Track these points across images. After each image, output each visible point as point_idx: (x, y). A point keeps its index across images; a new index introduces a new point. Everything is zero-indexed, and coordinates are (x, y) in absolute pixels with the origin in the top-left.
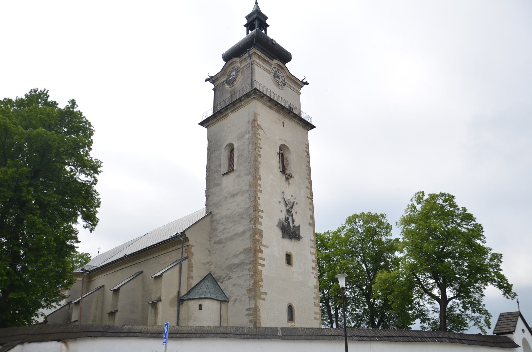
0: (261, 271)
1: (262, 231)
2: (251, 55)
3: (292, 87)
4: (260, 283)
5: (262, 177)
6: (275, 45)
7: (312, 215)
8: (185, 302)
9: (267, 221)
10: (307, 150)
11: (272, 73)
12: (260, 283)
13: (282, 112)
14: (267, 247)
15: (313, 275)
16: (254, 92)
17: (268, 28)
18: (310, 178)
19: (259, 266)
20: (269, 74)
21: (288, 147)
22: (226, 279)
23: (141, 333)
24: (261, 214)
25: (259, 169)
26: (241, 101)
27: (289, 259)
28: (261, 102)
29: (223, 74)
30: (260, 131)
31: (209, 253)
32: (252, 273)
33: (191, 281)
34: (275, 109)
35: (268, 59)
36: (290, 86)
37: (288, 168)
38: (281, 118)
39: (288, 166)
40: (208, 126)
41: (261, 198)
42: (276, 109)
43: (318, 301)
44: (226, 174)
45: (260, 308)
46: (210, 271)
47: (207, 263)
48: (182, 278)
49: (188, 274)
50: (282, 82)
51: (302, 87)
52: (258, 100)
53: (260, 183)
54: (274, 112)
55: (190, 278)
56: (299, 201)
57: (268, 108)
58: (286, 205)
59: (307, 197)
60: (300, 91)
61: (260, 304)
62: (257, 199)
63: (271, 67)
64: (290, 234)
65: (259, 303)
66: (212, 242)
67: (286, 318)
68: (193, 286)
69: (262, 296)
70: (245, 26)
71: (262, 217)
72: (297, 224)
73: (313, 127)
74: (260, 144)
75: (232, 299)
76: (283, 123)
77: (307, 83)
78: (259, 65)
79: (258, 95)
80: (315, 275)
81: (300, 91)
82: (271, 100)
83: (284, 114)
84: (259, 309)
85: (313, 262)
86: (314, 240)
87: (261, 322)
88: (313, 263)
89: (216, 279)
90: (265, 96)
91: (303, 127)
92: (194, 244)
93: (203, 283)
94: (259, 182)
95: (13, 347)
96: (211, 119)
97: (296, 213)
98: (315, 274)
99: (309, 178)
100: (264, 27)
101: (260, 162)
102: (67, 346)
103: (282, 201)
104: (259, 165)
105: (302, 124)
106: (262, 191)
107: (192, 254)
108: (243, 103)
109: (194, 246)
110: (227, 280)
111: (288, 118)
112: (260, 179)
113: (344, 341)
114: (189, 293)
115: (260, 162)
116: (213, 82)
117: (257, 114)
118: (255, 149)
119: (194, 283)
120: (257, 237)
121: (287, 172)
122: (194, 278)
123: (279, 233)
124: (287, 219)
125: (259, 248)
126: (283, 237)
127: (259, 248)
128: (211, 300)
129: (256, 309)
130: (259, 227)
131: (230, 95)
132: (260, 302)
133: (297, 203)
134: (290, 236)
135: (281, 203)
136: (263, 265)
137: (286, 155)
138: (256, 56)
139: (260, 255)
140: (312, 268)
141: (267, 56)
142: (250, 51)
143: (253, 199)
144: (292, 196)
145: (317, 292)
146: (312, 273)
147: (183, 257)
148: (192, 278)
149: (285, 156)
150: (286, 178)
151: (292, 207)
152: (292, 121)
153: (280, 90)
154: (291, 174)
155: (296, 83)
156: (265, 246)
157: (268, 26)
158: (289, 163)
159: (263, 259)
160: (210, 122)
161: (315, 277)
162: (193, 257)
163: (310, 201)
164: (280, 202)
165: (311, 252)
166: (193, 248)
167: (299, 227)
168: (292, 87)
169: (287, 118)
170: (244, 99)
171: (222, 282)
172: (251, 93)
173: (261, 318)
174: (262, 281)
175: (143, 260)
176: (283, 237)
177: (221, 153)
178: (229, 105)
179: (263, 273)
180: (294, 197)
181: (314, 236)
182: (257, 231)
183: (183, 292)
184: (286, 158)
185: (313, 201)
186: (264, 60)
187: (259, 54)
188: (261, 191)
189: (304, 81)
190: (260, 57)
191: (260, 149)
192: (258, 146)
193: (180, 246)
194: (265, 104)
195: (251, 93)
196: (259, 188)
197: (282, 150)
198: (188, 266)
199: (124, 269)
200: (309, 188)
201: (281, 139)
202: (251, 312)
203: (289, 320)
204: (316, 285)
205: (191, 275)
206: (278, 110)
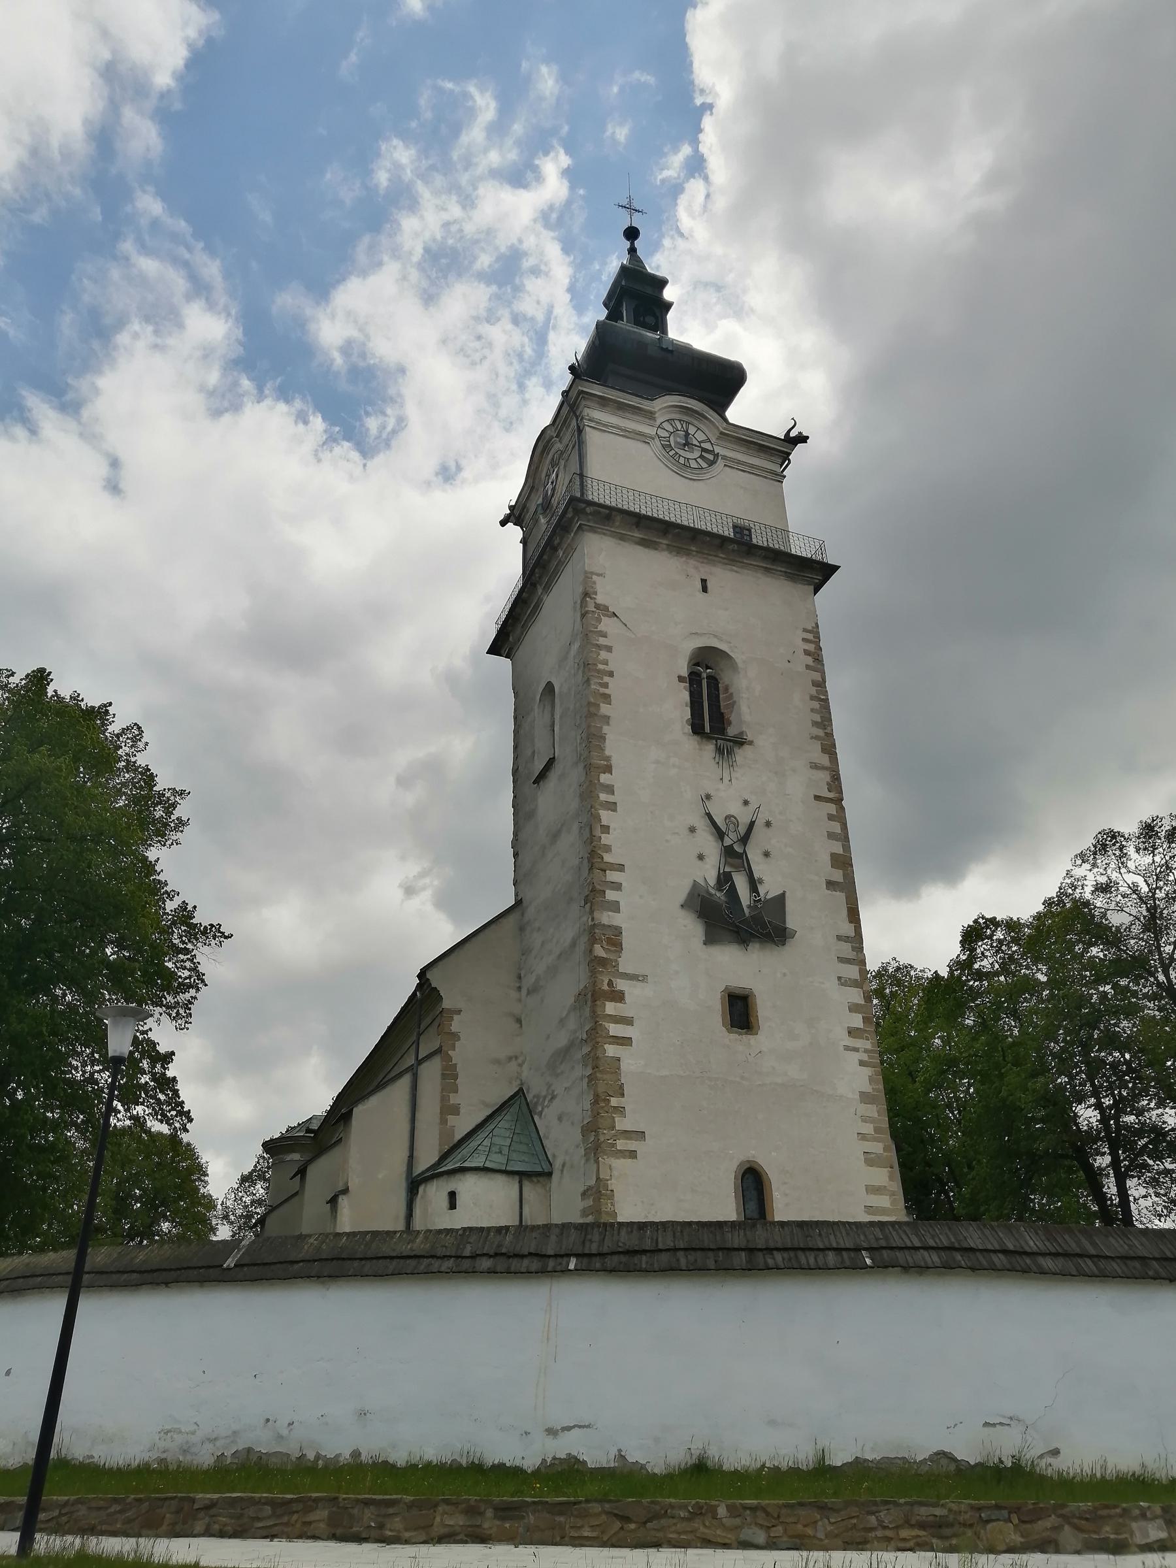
0: (619, 1060)
1: (618, 931)
3: (744, 463)
4: (614, 1102)
5: (613, 762)
6: (672, 351)
7: (841, 851)
9: (641, 897)
11: (657, 440)
12: (614, 1102)
13: (694, 549)
14: (642, 981)
15: (855, 1057)
16: (574, 509)
18: (830, 735)
19: (606, 1046)
20: (646, 445)
24: (612, 876)
25: (603, 738)
28: (611, 536)
29: (533, 487)
30: (606, 624)
31: (519, 1025)
32: (589, 1071)
34: (665, 546)
35: (633, 401)
36: (732, 464)
38: (696, 568)
39: (732, 712)
40: (511, 649)
41: (612, 826)
42: (667, 545)
45: (613, 1184)
46: (522, 1084)
47: (510, 1059)
49: (444, 1099)
50: (701, 457)
52: (595, 532)
53: (608, 783)
54: (666, 553)
55: (449, 1110)
58: (720, 834)
59: (817, 798)
61: (615, 1173)
62: (597, 832)
63: (654, 419)
64: (737, 927)
65: (611, 1169)
66: (524, 991)
68: (458, 1137)
69: (621, 1144)
71: (617, 887)
72: (769, 889)
77: (802, 439)
78: (604, 425)
79: (590, 517)
82: (639, 521)
83: (704, 554)
84: (610, 1188)
85: (850, 1010)
90: (614, 513)
94: (604, 778)
96: (510, 628)
98: (866, 1051)
101: (606, 719)
103: (702, 824)
105: (783, 569)
106: (616, 803)
107: (455, 1036)
108: (561, 553)
109: (459, 1012)
111: (725, 561)
112: (608, 769)
113: (68, 1290)
114: (444, 1157)
115: (609, 717)
117: (592, 573)
118: (588, 681)
119: (462, 1125)
120: (599, 951)
121: (731, 731)
122: (462, 1111)
123: (692, 928)
124: (724, 879)
125: (606, 987)
126: (711, 939)
127: (606, 987)
128: (482, 1173)
129: (600, 1191)
130: (606, 918)
132: (613, 1165)
134: (737, 933)
136: (626, 1041)
137: (725, 678)
138: (588, 403)
140: (849, 1032)
141: (617, 389)
143: (587, 834)
144: (746, 803)
145: (876, 1115)
146: (847, 1048)
148: (455, 1110)
149: (723, 683)
150: (719, 751)
151: (745, 839)
152: (742, 567)
153: (695, 483)
154: (742, 733)
156: (633, 977)
158: (735, 702)
159: (628, 1021)
161: (862, 1063)
163: (832, 808)
164: (692, 830)
165: (839, 978)
166: (456, 1017)
167: (781, 899)
169: (720, 562)
170: (561, 539)
174: (623, 1095)
176: (711, 939)
177: (534, 720)
179: (624, 1066)
182: (597, 931)
184: (727, 689)
185: (843, 809)
186: (621, 407)
187: (601, 394)
188: (612, 807)
189: (793, 434)
190: (603, 402)
191: (606, 679)
192: (599, 671)
194: (622, 538)
195: (569, 515)
196: (603, 797)
197: (708, 667)
200: (823, 768)
204: (868, 1088)
206: (674, 544)
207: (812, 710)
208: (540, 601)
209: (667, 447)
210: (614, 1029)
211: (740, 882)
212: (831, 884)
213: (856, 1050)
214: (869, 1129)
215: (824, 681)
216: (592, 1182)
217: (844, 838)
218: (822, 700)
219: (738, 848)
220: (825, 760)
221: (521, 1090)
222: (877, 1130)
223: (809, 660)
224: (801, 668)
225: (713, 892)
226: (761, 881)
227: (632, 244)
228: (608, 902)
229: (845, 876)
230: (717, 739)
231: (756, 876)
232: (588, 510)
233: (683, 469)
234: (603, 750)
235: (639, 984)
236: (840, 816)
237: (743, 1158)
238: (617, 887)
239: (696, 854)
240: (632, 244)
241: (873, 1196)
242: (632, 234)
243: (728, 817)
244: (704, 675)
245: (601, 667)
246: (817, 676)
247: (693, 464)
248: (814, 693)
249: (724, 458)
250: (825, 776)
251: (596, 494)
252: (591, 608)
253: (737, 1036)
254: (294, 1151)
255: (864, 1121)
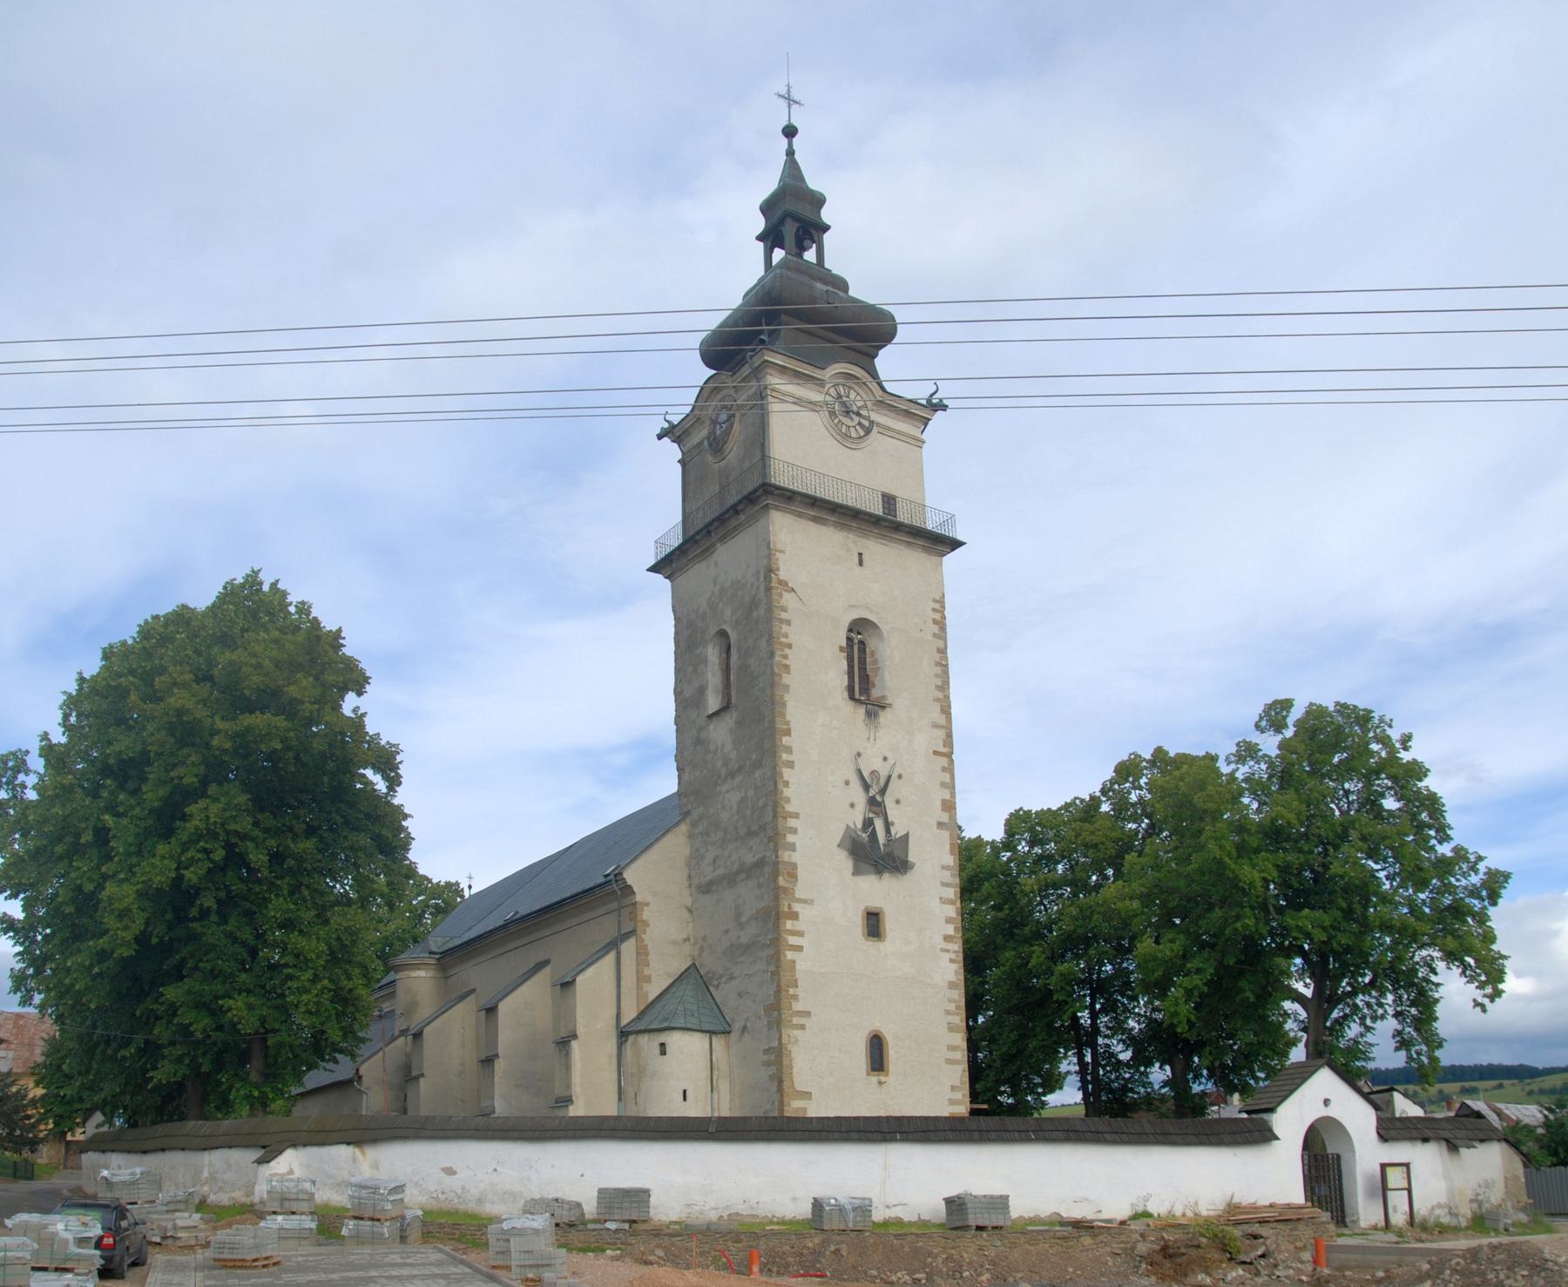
0: (794, 962)
1: (795, 866)
2: (757, 368)
5: (792, 725)
8: (631, 1038)
10: (937, 616)
12: (791, 991)
17: (827, 237)
18: (947, 697)
21: (875, 624)
22: (724, 980)
23: (477, 1130)
24: (792, 823)
26: (737, 512)
27: (874, 924)
33: (646, 987)
36: (886, 430)
37: (877, 681)
38: (854, 542)
39: (876, 676)
43: (959, 1018)
44: (716, 714)
48: (622, 983)
51: (929, 420)
54: (831, 528)
55: (642, 979)
56: (909, 767)
57: (811, 523)
58: (866, 787)
59: (935, 753)
60: (924, 437)
62: (780, 786)
67: (865, 1066)
68: (651, 999)
69: (796, 1020)
70: (759, 238)
71: (794, 831)
73: (955, 544)
74: (787, 637)
75: (737, 1026)
76: (860, 554)
80: (953, 956)
81: (924, 437)
86: (952, 864)
87: (795, 1079)
88: (948, 925)
89: (706, 979)
91: (927, 550)
92: (649, 899)
93: (674, 990)
95: (281, 1152)
97: (898, 802)
98: (954, 952)
99: (942, 697)
100: (814, 233)
102: (363, 1153)
103: (854, 779)
104: (786, 695)
108: (742, 517)
109: (648, 904)
110: (726, 983)
112: (788, 732)
114: (642, 1014)
116: (678, 440)
119: (653, 991)
121: (875, 693)
122: (653, 980)
123: (844, 862)
124: (868, 823)
125: (786, 909)
126: (857, 872)
127: (786, 909)
131: (717, 488)
133: (900, 777)
135: (852, 784)
136: (799, 949)
137: (872, 644)
139: (789, 924)
140: (945, 939)
142: (754, 358)
144: (885, 759)
145: (957, 997)
146: (943, 950)
147: (622, 932)
150: (869, 714)
151: (883, 792)
155: (907, 414)
156: (804, 901)
157: (826, 228)
158: (879, 668)
159: (800, 934)
160: (674, 565)
161: (951, 961)
162: (648, 929)
163: (944, 761)
164: (847, 783)
165: (941, 898)
166: (646, 908)
167: (906, 837)
168: (889, 429)
171: (717, 987)
172: (758, 494)
173: (795, 1070)
175: (547, 932)
176: (857, 872)
178: (711, 523)
179: (798, 967)
180: (891, 762)
181: (952, 854)
183: (629, 1014)
184: (873, 654)
185: (952, 761)
186: (798, 375)
190: (783, 370)
191: (787, 651)
193: (614, 905)
194: (800, 515)
197: (859, 633)
198: (637, 953)
199: (512, 953)
200: (942, 727)
201: (853, 606)
202: (773, 1057)
203: (873, 1069)
204: (953, 979)
205: (646, 973)
207: (936, 675)
208: (713, 545)
209: (832, 414)
210: (792, 940)
211: (879, 825)
212: (940, 825)
213: (948, 951)
214: (952, 1007)
215: (946, 648)
216: (776, 1044)
217: (951, 787)
218: (944, 666)
219: (879, 798)
220: (942, 720)
221: (694, 964)
222: (957, 1008)
223: (936, 629)
224: (930, 637)
225: (859, 833)
226: (893, 824)
227: (790, 145)
228: (788, 843)
229: (950, 817)
230: (866, 704)
231: (890, 820)
232: (776, 492)
233: (845, 438)
234: (784, 715)
235: (808, 906)
236: (949, 769)
237: (872, 1028)
238: (794, 831)
239: (849, 803)
240: (790, 145)
241: (951, 1053)
242: (790, 132)
243: (873, 772)
244: (856, 641)
245: (783, 640)
246: (940, 644)
247: (854, 434)
248: (938, 660)
249: (879, 425)
250: (941, 733)
251: (781, 477)
252: (774, 584)
253: (871, 943)
254: (419, 969)
255: (950, 1001)
